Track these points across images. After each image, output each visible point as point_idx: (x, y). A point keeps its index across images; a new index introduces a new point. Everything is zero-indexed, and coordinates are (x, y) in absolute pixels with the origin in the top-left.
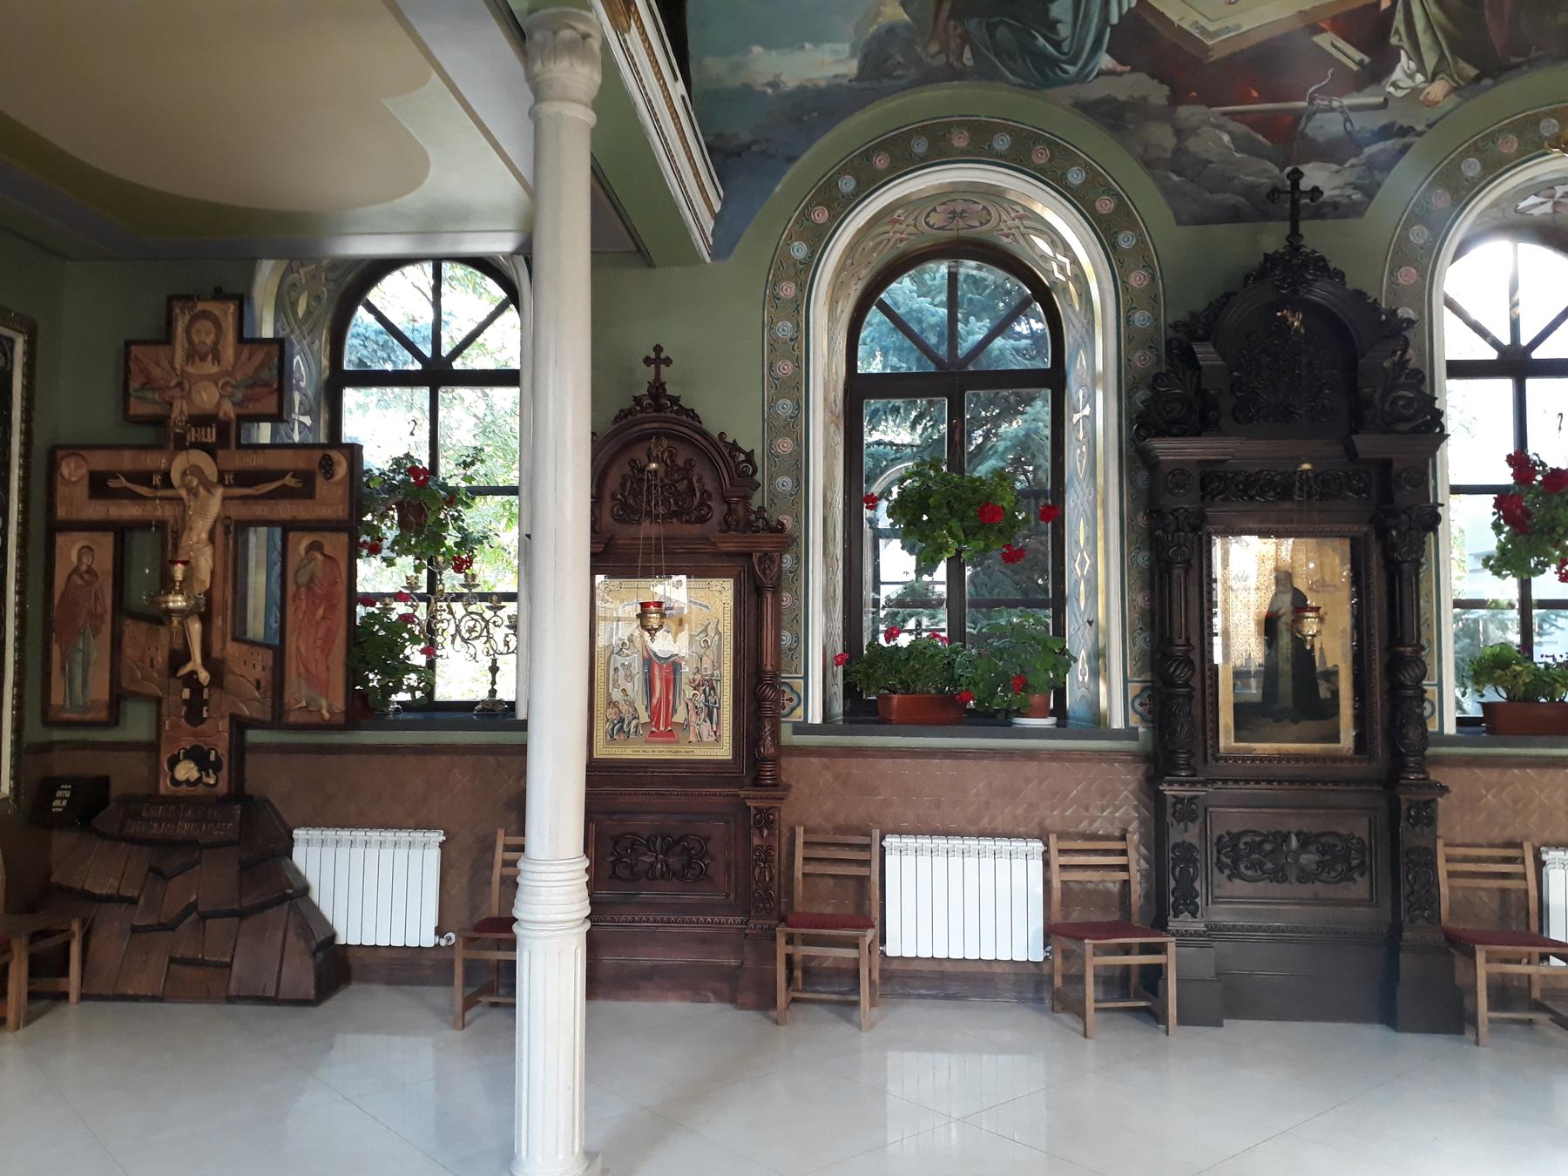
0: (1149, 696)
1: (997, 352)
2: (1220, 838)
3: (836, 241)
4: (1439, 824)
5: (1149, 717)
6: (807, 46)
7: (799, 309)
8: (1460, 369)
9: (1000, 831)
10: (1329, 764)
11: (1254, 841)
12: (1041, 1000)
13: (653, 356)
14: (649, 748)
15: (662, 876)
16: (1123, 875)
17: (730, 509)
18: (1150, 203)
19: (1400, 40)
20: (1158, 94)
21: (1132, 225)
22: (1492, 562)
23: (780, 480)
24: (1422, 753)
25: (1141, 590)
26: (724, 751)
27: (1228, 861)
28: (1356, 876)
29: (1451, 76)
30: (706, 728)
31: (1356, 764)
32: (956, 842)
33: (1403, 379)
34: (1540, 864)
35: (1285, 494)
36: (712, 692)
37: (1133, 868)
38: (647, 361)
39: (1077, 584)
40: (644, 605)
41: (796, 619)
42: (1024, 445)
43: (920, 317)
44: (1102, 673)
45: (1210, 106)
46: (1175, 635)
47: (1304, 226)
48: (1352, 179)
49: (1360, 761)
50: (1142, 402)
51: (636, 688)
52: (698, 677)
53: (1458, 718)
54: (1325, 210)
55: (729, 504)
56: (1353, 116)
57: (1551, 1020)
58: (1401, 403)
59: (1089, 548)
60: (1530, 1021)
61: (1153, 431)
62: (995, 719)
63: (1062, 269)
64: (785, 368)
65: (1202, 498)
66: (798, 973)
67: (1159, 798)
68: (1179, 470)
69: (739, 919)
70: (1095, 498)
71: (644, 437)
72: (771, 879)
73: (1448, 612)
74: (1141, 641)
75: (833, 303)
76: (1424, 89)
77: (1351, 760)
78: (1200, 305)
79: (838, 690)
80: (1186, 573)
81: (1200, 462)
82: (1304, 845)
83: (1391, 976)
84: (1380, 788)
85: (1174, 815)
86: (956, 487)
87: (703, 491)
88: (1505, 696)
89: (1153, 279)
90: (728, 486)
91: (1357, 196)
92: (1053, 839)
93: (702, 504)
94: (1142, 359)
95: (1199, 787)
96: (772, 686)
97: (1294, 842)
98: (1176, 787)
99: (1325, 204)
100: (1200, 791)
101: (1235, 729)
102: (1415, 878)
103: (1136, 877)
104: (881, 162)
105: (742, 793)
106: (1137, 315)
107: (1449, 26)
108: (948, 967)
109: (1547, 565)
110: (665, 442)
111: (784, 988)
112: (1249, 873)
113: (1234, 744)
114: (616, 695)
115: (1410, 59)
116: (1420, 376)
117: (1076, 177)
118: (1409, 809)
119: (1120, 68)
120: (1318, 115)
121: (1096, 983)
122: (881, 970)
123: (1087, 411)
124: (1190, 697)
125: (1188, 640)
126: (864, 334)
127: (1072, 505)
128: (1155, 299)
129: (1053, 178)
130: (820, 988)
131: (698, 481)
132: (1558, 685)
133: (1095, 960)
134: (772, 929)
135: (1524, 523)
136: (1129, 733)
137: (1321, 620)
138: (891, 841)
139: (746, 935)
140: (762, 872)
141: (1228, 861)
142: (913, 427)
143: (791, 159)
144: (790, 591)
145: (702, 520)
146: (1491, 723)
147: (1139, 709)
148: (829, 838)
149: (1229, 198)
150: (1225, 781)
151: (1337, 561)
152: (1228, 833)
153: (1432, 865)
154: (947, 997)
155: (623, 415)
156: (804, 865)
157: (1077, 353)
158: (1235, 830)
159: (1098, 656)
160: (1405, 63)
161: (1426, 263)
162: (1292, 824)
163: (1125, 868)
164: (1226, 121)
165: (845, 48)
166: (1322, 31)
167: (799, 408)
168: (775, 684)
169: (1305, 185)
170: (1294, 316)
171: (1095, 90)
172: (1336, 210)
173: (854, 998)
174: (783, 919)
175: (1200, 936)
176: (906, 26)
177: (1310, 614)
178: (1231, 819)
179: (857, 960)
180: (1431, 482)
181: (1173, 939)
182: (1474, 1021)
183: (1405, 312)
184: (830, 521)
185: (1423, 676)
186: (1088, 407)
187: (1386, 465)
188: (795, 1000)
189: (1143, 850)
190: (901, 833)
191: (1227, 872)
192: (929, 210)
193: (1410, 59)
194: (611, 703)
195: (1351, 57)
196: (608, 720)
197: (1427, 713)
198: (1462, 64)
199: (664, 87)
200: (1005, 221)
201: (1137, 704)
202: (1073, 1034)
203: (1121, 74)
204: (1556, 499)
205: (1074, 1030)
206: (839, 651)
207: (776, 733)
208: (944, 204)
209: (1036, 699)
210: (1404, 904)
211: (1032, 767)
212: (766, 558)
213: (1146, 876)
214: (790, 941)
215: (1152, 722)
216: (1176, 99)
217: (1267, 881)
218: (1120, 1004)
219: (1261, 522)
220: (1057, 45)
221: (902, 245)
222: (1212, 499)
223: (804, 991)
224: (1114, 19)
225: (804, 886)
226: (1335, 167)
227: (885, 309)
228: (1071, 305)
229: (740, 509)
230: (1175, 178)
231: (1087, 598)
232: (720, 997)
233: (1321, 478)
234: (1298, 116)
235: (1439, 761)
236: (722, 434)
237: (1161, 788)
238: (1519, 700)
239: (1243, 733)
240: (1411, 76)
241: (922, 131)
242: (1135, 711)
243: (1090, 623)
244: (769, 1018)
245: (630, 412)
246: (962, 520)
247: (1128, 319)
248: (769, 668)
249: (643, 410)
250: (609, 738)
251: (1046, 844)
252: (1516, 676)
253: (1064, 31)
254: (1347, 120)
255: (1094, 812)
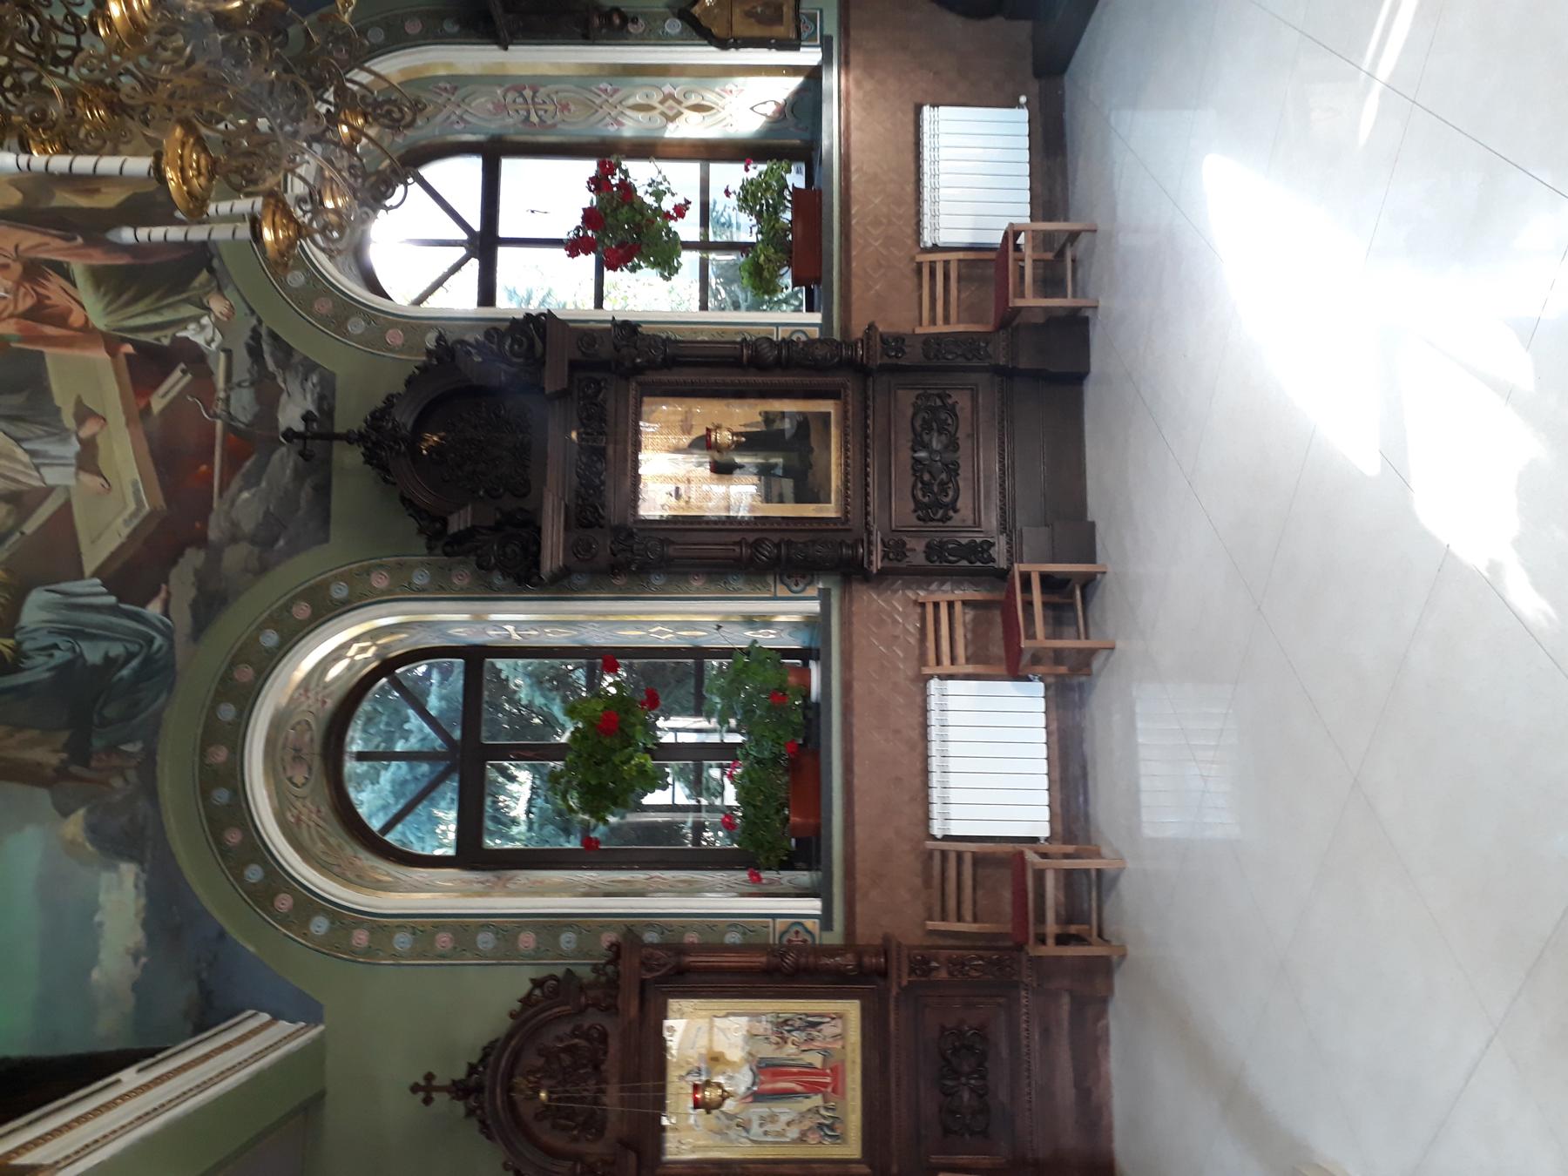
0: (789, 577)
1: (444, 704)
2: (919, 518)
3: (308, 881)
4: (901, 330)
5: (809, 578)
6: (97, 918)
7: (381, 925)
8: (487, 294)
9: (921, 719)
10: (850, 423)
11: (921, 489)
12: (1081, 685)
13: (421, 1095)
14: (850, 1095)
15: (983, 1078)
16: (958, 607)
17: (593, 1005)
18: (304, 568)
19: (166, 336)
20: (193, 558)
21: (324, 586)
22: (666, 274)
23: (564, 945)
24: (839, 345)
25: (688, 582)
26: (851, 1009)
27: (941, 512)
28: (950, 401)
29: (207, 293)
30: (828, 1029)
31: (849, 399)
32: (935, 763)
33: (494, 347)
34: (936, 248)
35: (601, 453)
36: (790, 1023)
37: (951, 597)
38: (427, 1101)
39: (679, 637)
40: (697, 1105)
41: (712, 927)
42: (537, 680)
43: (399, 786)
44: (767, 619)
45: (210, 508)
46: (731, 554)
47: (340, 427)
48: (297, 383)
49: (846, 396)
50: (504, 579)
51: (785, 1111)
52: (774, 1039)
53: (807, 311)
54: (325, 407)
55: (587, 1006)
56: (235, 379)
57: (1072, 245)
58: (516, 347)
59: (645, 627)
60: (1074, 261)
61: (534, 570)
62: (814, 714)
63: (363, 650)
64: (444, 940)
65: (601, 527)
66: (1073, 929)
67: (883, 573)
68: (572, 548)
69: (1023, 993)
70: (598, 622)
71: (511, 1105)
72: (981, 958)
73: (712, 316)
74: (737, 583)
75: (380, 886)
76: (217, 318)
77: (846, 403)
78: (412, 525)
79: (786, 876)
80: (673, 543)
81: (567, 528)
82: (926, 446)
83: (1039, 377)
84: (871, 379)
85: (899, 561)
86: (579, 756)
87: (573, 1035)
88: (786, 268)
89: (381, 566)
90: (568, 1007)
91: (315, 379)
92: (926, 671)
93: (586, 1036)
94: (461, 579)
95: (873, 538)
96: (783, 956)
97: (922, 454)
98: (874, 558)
99: (320, 409)
100: (877, 538)
101: (819, 503)
102: (951, 353)
103: (959, 594)
104: (234, 837)
105: (894, 991)
106: (417, 581)
107: (154, 296)
108: (1056, 775)
109: (669, 230)
110: (518, 1080)
111: (1086, 948)
112: (951, 493)
113: (833, 505)
114: (793, 1133)
115: (186, 328)
116: (492, 332)
117: (270, 639)
118: (890, 357)
119: (163, 595)
120: (232, 412)
121: (1060, 637)
122: (1064, 843)
123: (510, 628)
124: (789, 543)
125: (735, 543)
126: (417, 849)
127: (603, 641)
128: (401, 565)
129: (267, 663)
130: (1086, 906)
131: (561, 1041)
132: (777, 225)
133: (1040, 637)
134: (1030, 959)
135: (630, 247)
136: (824, 597)
137: (718, 427)
138: (937, 829)
139: (1039, 985)
140: (975, 968)
141: (941, 512)
142: (512, 779)
143: (222, 935)
144: (683, 934)
145: (604, 1037)
146: (812, 281)
147: (801, 586)
148: (937, 893)
149: (306, 492)
150: (867, 514)
151: (664, 407)
152: (915, 511)
153: (939, 337)
154: (1085, 775)
155: (485, 1128)
156: (964, 921)
157: (450, 635)
158: (912, 506)
159: (750, 621)
160: (190, 333)
161: (383, 321)
162: (903, 456)
163: (951, 605)
164: (228, 494)
165: (106, 877)
166: (148, 406)
167: (487, 925)
168: (779, 951)
169: (299, 426)
170: (427, 440)
171: (182, 619)
172: (326, 399)
173: (1094, 874)
174: (1020, 947)
175: (1011, 540)
176: (90, 812)
177: (713, 437)
178: (902, 510)
179: (1057, 871)
180: (592, 325)
181: (1016, 565)
182: (1076, 310)
183: (430, 341)
184: (610, 889)
185: (770, 340)
186: (506, 627)
187: (574, 366)
188: (1100, 935)
189: (934, 587)
190: (927, 819)
191: (951, 513)
192: (289, 783)
193: (186, 328)
194: (802, 1139)
195: (177, 380)
196: (820, 1143)
197: (803, 338)
198: (196, 283)
199: (124, 1098)
200: (310, 706)
201: (795, 588)
202: (1112, 659)
203: (169, 593)
204: (610, 220)
205: (1107, 659)
206: (744, 875)
207: (831, 951)
208: (284, 769)
209: (792, 679)
210: (975, 363)
211: (857, 687)
212: (645, 964)
213: (958, 584)
214: (1042, 940)
215: (813, 575)
216: (201, 541)
217: (958, 478)
218: (1080, 613)
219: (626, 474)
220: (130, 656)
221: (325, 809)
222: (603, 518)
223: (1088, 922)
224: (112, 599)
225: (983, 922)
226: (284, 397)
227: (388, 827)
228: (401, 640)
229: (592, 993)
230: (281, 543)
231: (695, 630)
232: (1102, 1014)
233: (585, 421)
234: (229, 428)
235: (845, 329)
236: (512, 1015)
237: (875, 571)
238: (791, 258)
239: (822, 496)
240: (203, 328)
241: (205, 794)
242: (803, 590)
243: (719, 627)
244: (1119, 964)
245: (483, 1122)
246: (614, 751)
247: (420, 590)
248: (764, 959)
249: (481, 1107)
250: (839, 1141)
251: (931, 677)
252: (768, 259)
253: (117, 650)
254: (239, 385)
255: (898, 632)
